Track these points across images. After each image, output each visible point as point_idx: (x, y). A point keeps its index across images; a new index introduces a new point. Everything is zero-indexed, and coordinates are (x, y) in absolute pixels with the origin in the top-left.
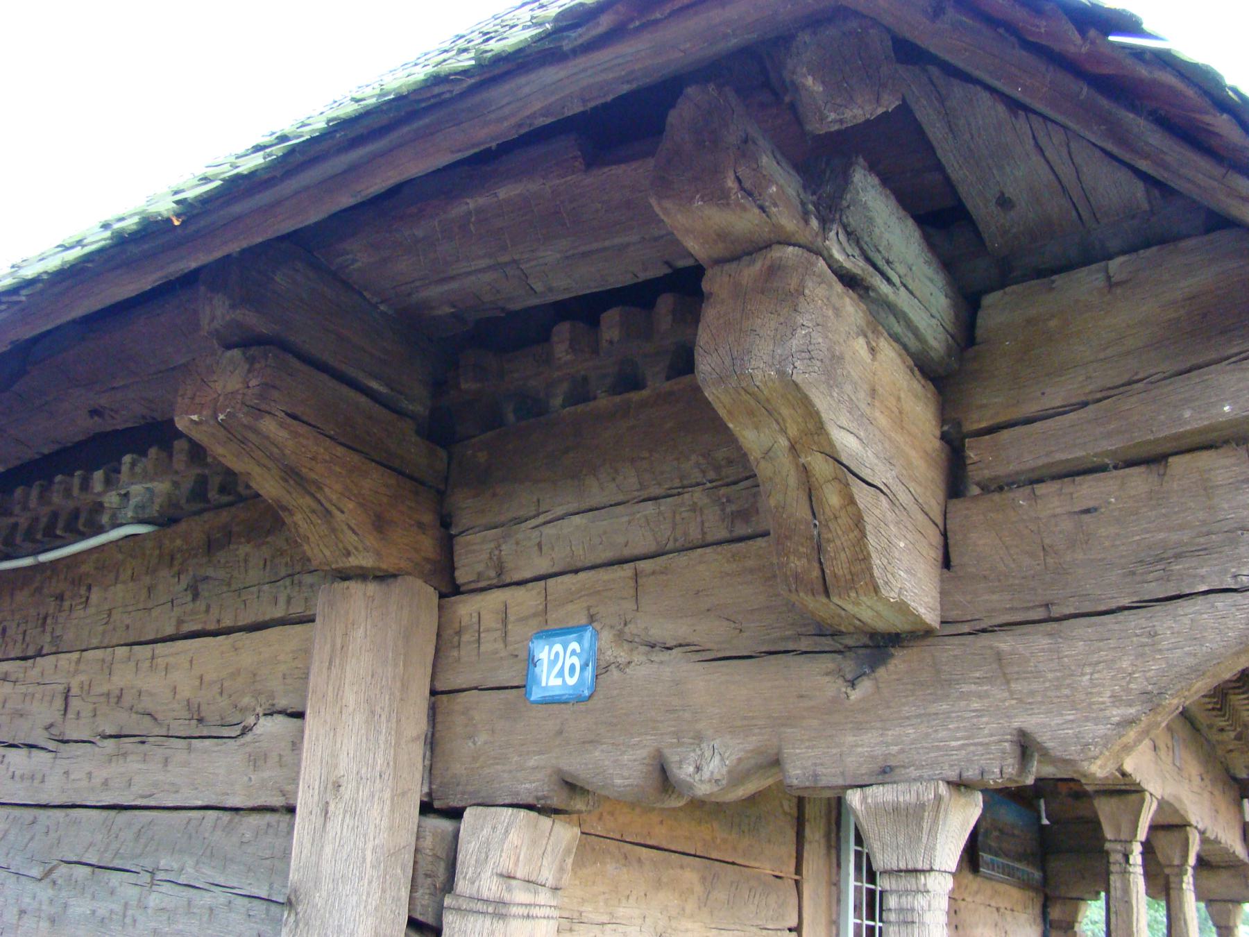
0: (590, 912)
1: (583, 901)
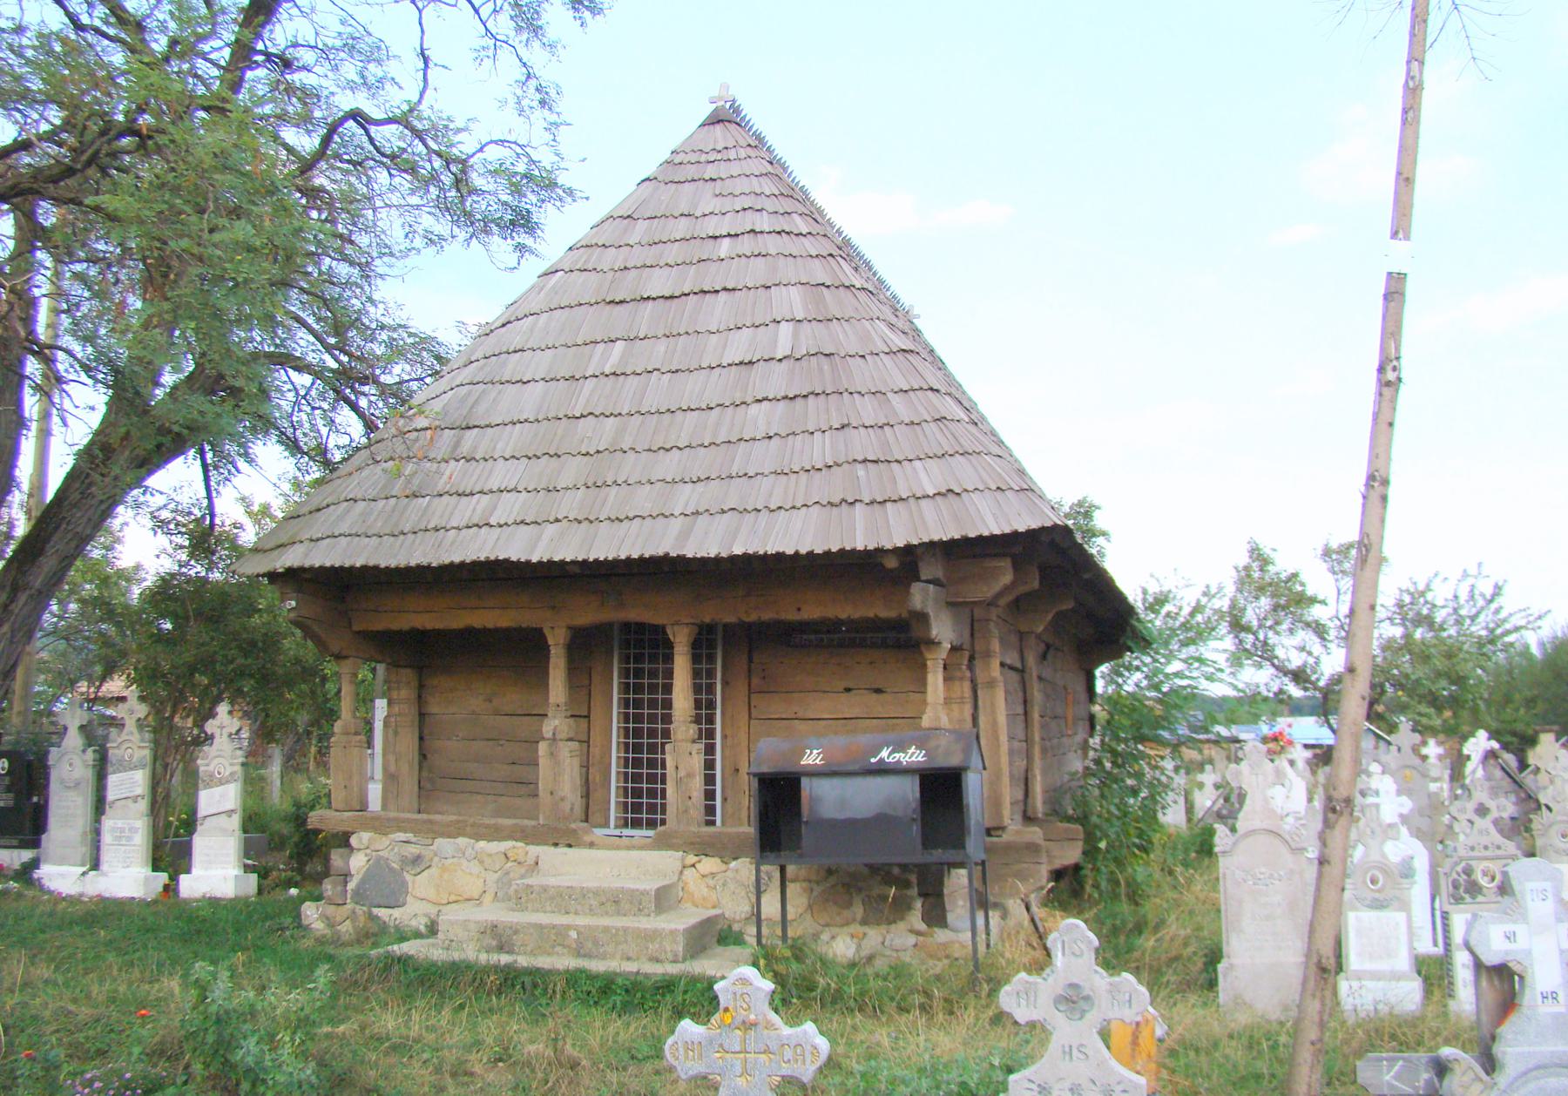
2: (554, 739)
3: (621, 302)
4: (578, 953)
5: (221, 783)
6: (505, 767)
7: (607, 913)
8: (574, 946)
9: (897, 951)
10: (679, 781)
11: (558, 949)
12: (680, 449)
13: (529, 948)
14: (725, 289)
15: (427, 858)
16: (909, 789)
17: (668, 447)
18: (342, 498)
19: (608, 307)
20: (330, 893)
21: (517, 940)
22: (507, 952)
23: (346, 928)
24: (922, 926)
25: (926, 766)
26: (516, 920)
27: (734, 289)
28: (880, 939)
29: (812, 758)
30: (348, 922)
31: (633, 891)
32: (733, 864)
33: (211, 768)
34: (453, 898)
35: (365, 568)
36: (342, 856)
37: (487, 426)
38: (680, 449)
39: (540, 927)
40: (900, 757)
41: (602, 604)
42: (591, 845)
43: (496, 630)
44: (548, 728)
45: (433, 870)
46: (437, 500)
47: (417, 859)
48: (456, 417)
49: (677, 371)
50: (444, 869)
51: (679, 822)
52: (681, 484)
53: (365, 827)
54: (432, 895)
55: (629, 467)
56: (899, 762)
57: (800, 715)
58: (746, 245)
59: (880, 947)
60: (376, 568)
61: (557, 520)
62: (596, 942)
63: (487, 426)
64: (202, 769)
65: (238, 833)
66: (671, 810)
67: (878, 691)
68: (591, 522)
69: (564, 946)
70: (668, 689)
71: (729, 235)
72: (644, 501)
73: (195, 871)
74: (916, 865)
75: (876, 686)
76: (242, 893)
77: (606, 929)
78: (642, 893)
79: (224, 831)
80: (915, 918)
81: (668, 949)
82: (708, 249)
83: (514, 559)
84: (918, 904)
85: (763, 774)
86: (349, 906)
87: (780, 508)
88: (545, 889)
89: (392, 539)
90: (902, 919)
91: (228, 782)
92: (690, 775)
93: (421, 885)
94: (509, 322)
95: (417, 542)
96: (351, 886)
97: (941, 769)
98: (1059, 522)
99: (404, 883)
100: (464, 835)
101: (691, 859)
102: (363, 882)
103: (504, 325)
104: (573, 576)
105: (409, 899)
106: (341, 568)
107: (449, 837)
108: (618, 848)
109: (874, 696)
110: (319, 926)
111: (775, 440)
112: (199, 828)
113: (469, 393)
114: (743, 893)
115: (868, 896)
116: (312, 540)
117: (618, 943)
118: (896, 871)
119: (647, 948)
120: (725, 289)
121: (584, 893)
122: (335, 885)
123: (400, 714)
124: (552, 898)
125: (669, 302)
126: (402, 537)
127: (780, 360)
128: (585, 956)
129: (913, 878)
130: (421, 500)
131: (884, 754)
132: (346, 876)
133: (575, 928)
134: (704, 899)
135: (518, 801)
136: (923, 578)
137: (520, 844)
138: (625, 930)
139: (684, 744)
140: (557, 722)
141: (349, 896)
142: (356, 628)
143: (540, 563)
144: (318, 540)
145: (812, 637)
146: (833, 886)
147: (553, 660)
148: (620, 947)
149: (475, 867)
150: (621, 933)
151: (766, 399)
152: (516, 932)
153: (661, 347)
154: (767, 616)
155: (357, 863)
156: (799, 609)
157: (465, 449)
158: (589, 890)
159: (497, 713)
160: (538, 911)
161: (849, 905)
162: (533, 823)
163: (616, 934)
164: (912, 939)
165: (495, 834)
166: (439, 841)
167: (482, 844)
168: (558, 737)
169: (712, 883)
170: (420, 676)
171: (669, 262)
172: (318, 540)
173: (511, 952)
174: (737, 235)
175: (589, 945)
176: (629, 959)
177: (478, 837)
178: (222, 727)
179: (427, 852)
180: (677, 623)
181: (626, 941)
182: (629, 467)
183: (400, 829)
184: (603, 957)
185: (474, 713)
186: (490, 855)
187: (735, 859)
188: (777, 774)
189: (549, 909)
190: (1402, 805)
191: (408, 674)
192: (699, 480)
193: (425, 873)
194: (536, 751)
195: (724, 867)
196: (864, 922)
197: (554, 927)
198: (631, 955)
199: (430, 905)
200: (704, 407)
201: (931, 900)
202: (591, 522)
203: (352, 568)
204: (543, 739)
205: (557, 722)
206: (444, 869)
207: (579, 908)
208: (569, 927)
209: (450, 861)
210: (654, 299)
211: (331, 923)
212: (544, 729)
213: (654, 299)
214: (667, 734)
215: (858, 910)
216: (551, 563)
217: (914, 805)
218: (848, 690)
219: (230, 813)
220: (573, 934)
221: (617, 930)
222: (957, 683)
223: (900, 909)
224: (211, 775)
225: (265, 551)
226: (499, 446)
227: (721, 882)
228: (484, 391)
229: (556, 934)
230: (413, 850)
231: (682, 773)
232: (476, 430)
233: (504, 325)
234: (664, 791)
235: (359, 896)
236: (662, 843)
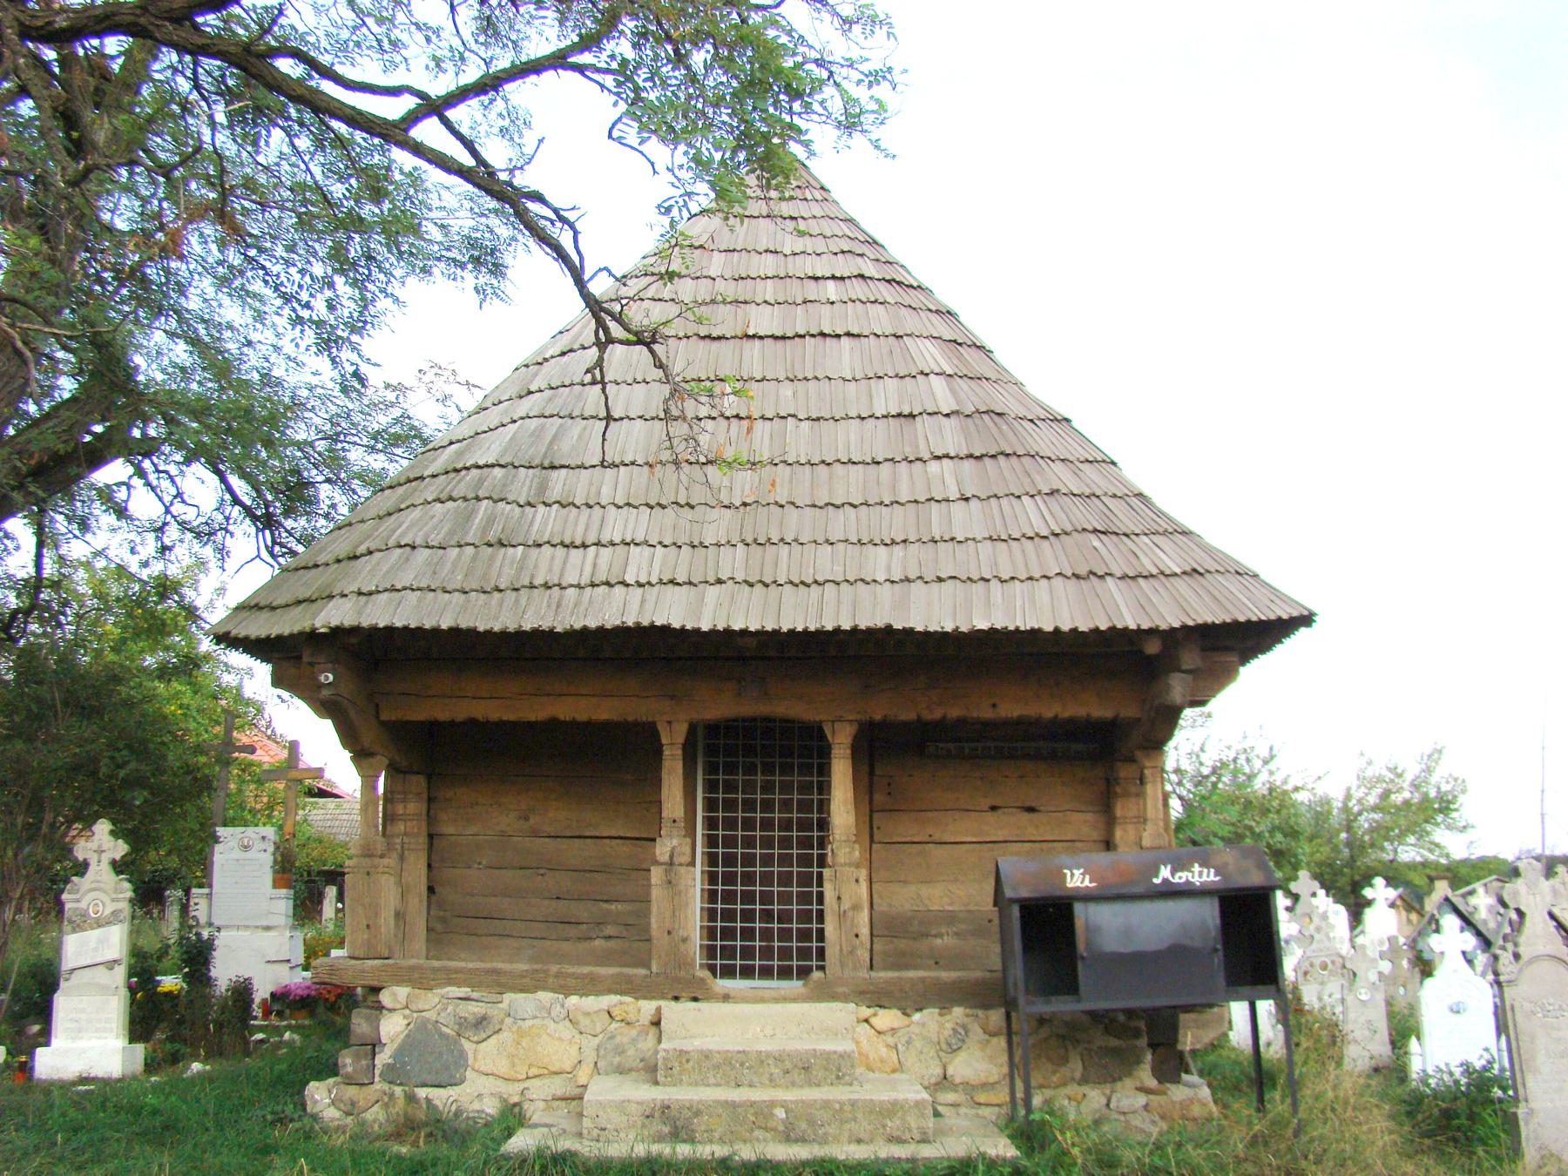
2: (671, 864)
3: (719, 338)
4: (788, 1137)
5: (100, 923)
6: (547, 902)
7: (793, 1084)
8: (781, 1128)
9: (1124, 1113)
10: (842, 916)
11: (757, 1133)
12: (855, 506)
13: (717, 1135)
14: (848, 334)
15: (495, 1021)
16: (1208, 914)
17: (838, 502)
18: (391, 543)
19: (702, 343)
20: (350, 1069)
21: (700, 1124)
22: (685, 1141)
23: (375, 1115)
24: (1152, 1083)
25: (1222, 886)
26: (696, 1098)
27: (859, 336)
28: (1104, 1101)
29: (1077, 880)
30: (376, 1108)
31: (829, 1053)
32: (917, 1016)
33: (83, 905)
34: (534, 1071)
35: (455, 631)
36: (368, 1018)
37: (579, 467)
38: (855, 506)
39: (733, 1105)
40: (1181, 877)
41: (739, 695)
42: (726, 998)
43: (589, 724)
44: (662, 849)
45: (504, 1035)
46: (534, 552)
47: (481, 1022)
48: (537, 453)
49: (818, 419)
50: (521, 1033)
51: (842, 965)
52: (870, 546)
53: (400, 981)
54: (503, 1067)
55: (795, 523)
56: (1188, 882)
57: (937, 837)
58: (857, 289)
59: (1104, 1110)
60: (472, 632)
61: (720, 582)
62: (811, 1122)
63: (579, 467)
64: (68, 906)
65: (124, 993)
66: (832, 952)
67: (1031, 810)
68: (767, 586)
69: (766, 1129)
70: (824, 806)
71: (833, 277)
72: (826, 563)
73: (55, 1042)
74: (1145, 1010)
75: (1028, 804)
76: (129, 1071)
77: (826, 1104)
78: (841, 1056)
79: (103, 989)
80: (1145, 1075)
81: (913, 1125)
82: (812, 290)
83: (676, 625)
84: (1149, 1057)
85: (1026, 899)
86: (380, 1085)
87: (1013, 578)
88: (707, 1055)
89: (483, 596)
90: (1129, 1074)
91: (109, 923)
92: (856, 907)
93: (486, 1054)
94: (571, 351)
95: (523, 601)
96: (383, 1058)
97: (1240, 889)
98: (1263, 618)
99: (462, 1054)
100: (545, 989)
101: (865, 1012)
102: (399, 1053)
103: (563, 354)
104: (742, 659)
105: (469, 1074)
106: (419, 629)
107: (522, 991)
108: (762, 1000)
109: (1026, 816)
110: (331, 1114)
111: (974, 503)
112: (63, 984)
113: (542, 428)
114: (932, 1053)
115: (1089, 1050)
116: (360, 593)
117: (842, 1122)
118: (1122, 1018)
119: (884, 1126)
120: (848, 334)
121: (762, 1059)
122: (357, 1058)
123: (405, 834)
124: (717, 1067)
125: (780, 343)
126: (496, 595)
127: (947, 415)
128: (796, 1141)
129: (1142, 1025)
130: (511, 550)
131: (1165, 872)
132: (374, 1045)
133: (784, 1105)
134: (882, 1061)
135: (566, 946)
136: (1184, 667)
137: (628, 999)
138: (853, 1103)
139: (846, 869)
140: (675, 842)
141: (377, 1072)
142: (384, 717)
143: (714, 632)
144: (370, 594)
145: (951, 746)
146: (1046, 1039)
147: (666, 764)
148: (847, 1126)
149: (565, 1030)
150: (847, 1108)
151: (947, 456)
152: (698, 1113)
153: (787, 390)
154: (954, 713)
155: (392, 1028)
156: (994, 706)
157: (555, 493)
158: (768, 1054)
159: (535, 834)
160: (696, 1084)
161: (1065, 1060)
162: (642, 971)
163: (841, 1109)
164: (1141, 1099)
165: (590, 986)
166: (509, 997)
167: (574, 999)
168: (677, 860)
169: (891, 1040)
170: (429, 783)
171: (768, 299)
172: (370, 594)
173: (691, 1140)
174: (842, 278)
175: (804, 1125)
176: (859, 1141)
177: (567, 991)
178: (100, 852)
179: (493, 1011)
180: (840, 720)
181: (855, 1119)
182: (795, 523)
183: (451, 982)
184: (824, 1141)
185: (503, 834)
186: (587, 1014)
187: (920, 1010)
188: (1043, 898)
189: (712, 1080)
190: (1465, 942)
191: (418, 782)
192: (893, 542)
193: (493, 1040)
194: (649, 880)
195: (905, 1020)
196: (1084, 1080)
197: (753, 1104)
198: (862, 1135)
199: (500, 1082)
200: (869, 460)
201: (1161, 1050)
202: (767, 586)
203: (436, 631)
204: (657, 863)
205: (675, 842)
206: (521, 1033)
207: (755, 1079)
208: (773, 1104)
209: (528, 1023)
210: (761, 338)
211: (351, 1109)
212: (658, 852)
213: (761, 338)
214: (822, 862)
215: (1076, 1066)
216: (728, 633)
217: (1213, 934)
218: (994, 808)
219: (111, 964)
220: (780, 1113)
221: (842, 1104)
222: (1133, 800)
223: (1123, 1063)
224: (84, 914)
225: (274, 609)
226: (604, 490)
227: (904, 1040)
228: (561, 425)
229: (756, 1114)
230: (474, 1009)
231: (846, 905)
232: (564, 471)
233: (563, 354)
234: (821, 932)
235: (394, 1074)
236: (826, 993)
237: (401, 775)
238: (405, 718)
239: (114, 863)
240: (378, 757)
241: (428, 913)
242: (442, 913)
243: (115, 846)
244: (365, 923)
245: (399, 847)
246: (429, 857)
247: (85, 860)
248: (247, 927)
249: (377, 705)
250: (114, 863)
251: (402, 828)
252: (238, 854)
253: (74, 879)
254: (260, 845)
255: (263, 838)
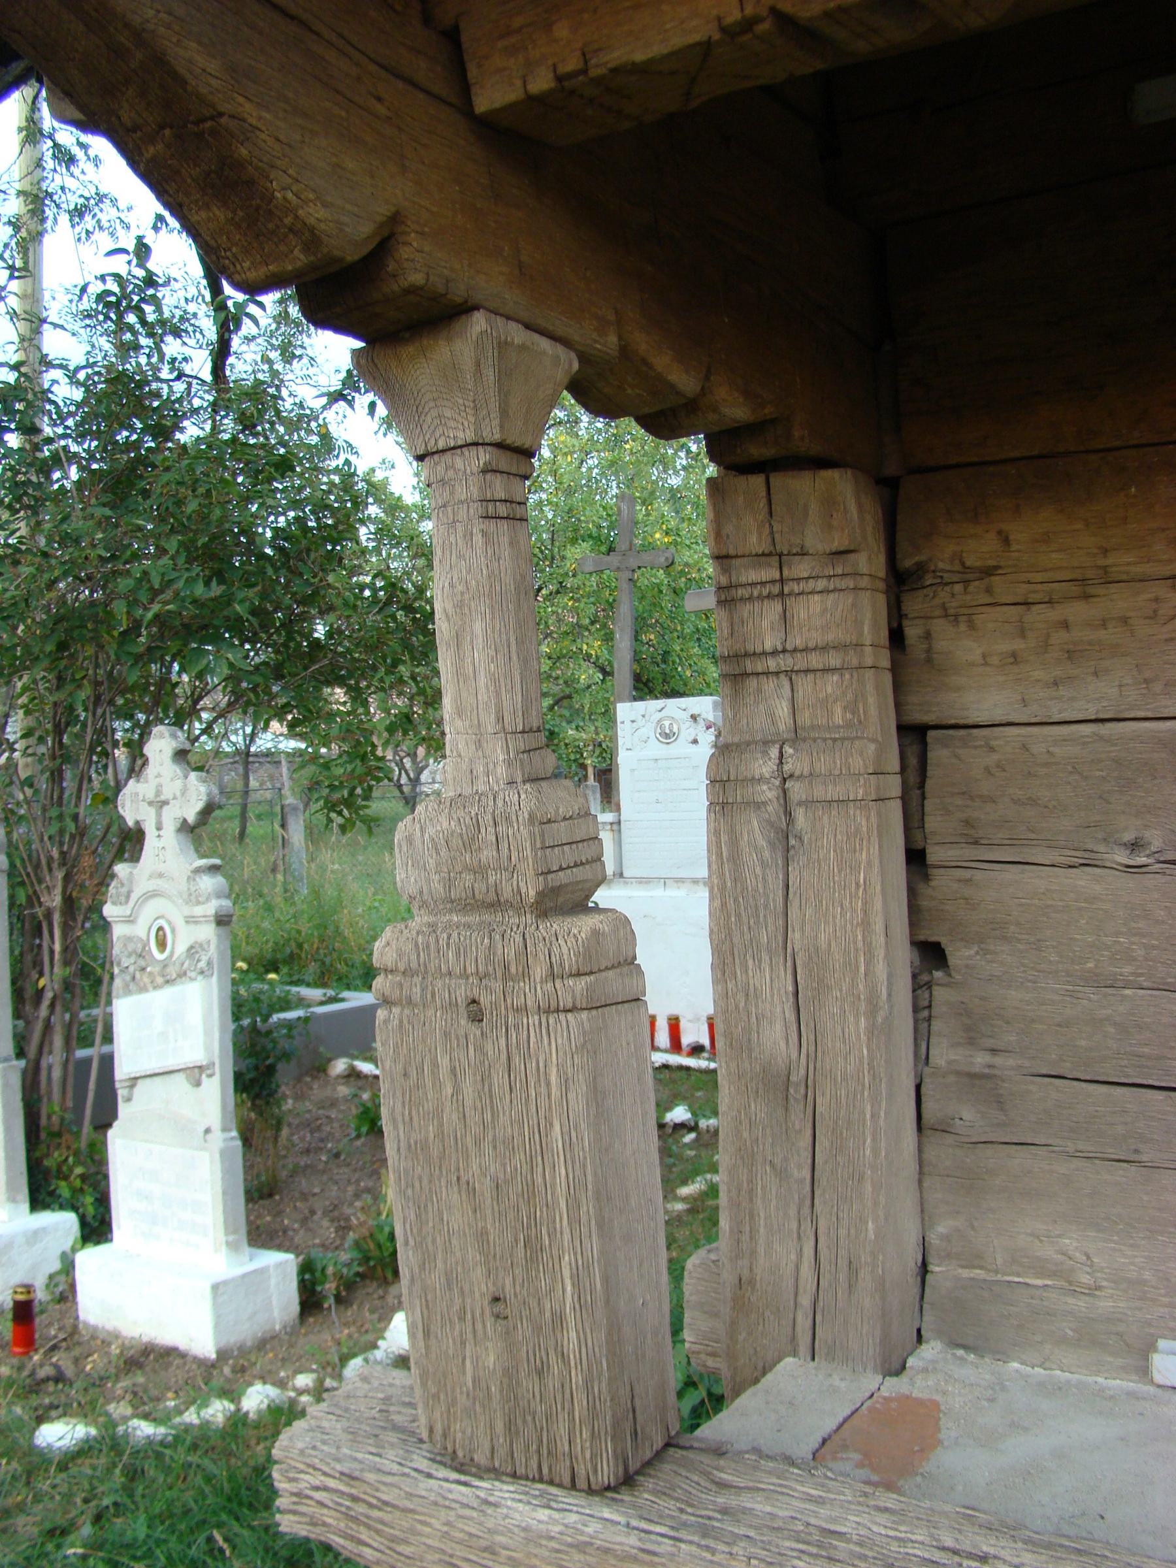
0: (1135, 563)
1: (1105, 552)
123: (797, 736)
219: (196, 1074)
237: (758, 481)
238: (601, 64)
239: (186, 828)
240: (479, 322)
241: (923, 1059)
242: (981, 1060)
243: (184, 791)
244: (480, 1287)
245: (768, 793)
246: (913, 820)
247: (137, 823)
248: (680, 881)
249: (452, 36)
250: (186, 828)
251: (783, 710)
252: (656, 749)
253: (121, 869)
254: (688, 731)
255: (694, 718)
